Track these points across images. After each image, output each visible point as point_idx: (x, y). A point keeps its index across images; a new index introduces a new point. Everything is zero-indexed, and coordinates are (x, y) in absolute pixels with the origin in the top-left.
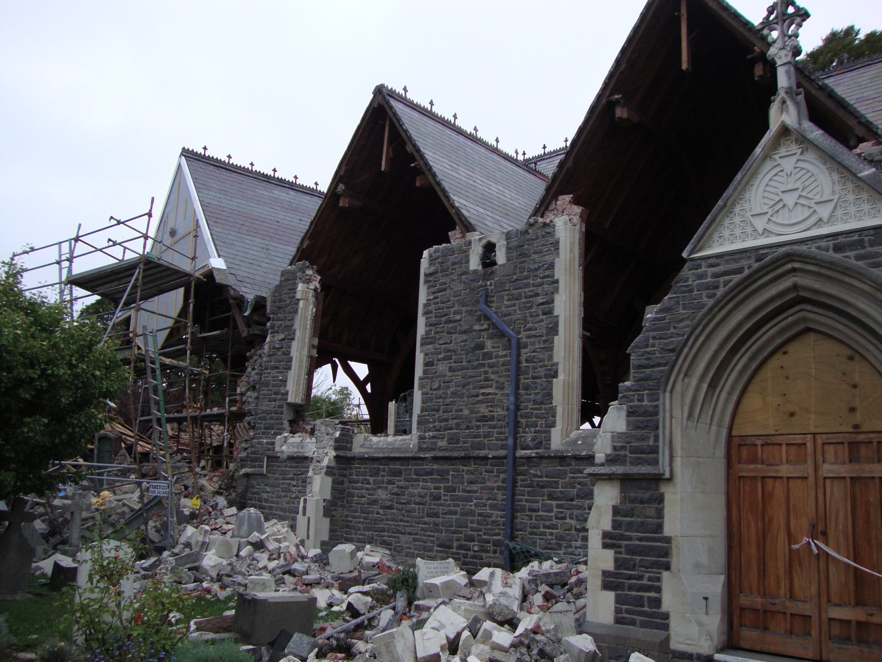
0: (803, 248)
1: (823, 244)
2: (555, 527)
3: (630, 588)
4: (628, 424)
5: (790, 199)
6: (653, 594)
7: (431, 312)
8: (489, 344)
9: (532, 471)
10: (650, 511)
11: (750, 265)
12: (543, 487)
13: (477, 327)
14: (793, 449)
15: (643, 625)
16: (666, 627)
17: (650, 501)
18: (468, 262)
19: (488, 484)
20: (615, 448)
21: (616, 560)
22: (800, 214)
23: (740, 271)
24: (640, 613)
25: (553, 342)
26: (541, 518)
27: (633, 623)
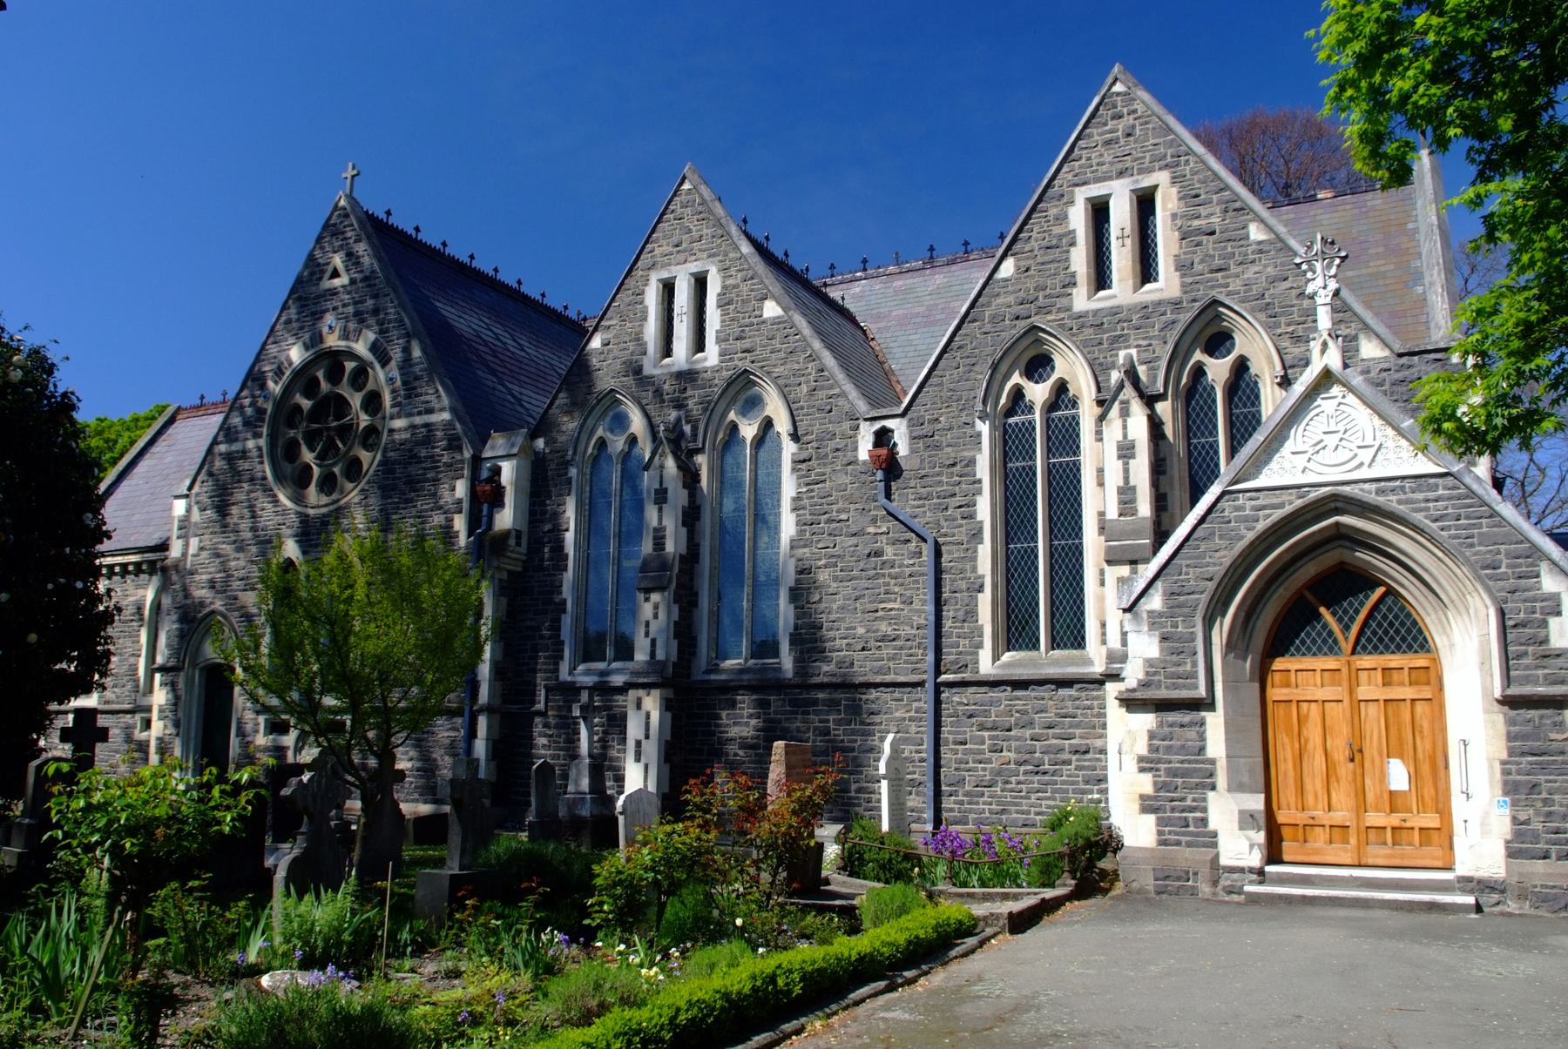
0: (1347, 489)
1: (1367, 486)
2: (989, 761)
3: (1173, 810)
4: (1162, 650)
5: (1331, 441)
6: (1198, 815)
7: (804, 508)
8: (889, 551)
9: (956, 699)
10: (1192, 734)
11: (1295, 503)
12: (971, 716)
13: (871, 530)
14: (1326, 674)
15: (1189, 844)
16: (1215, 845)
17: (1192, 724)
18: (856, 449)
19: (898, 714)
20: (1147, 673)
21: (1155, 783)
22: (1343, 455)
23: (1281, 506)
24: (1184, 834)
25: (976, 551)
26: (971, 751)
27: (1178, 843)
